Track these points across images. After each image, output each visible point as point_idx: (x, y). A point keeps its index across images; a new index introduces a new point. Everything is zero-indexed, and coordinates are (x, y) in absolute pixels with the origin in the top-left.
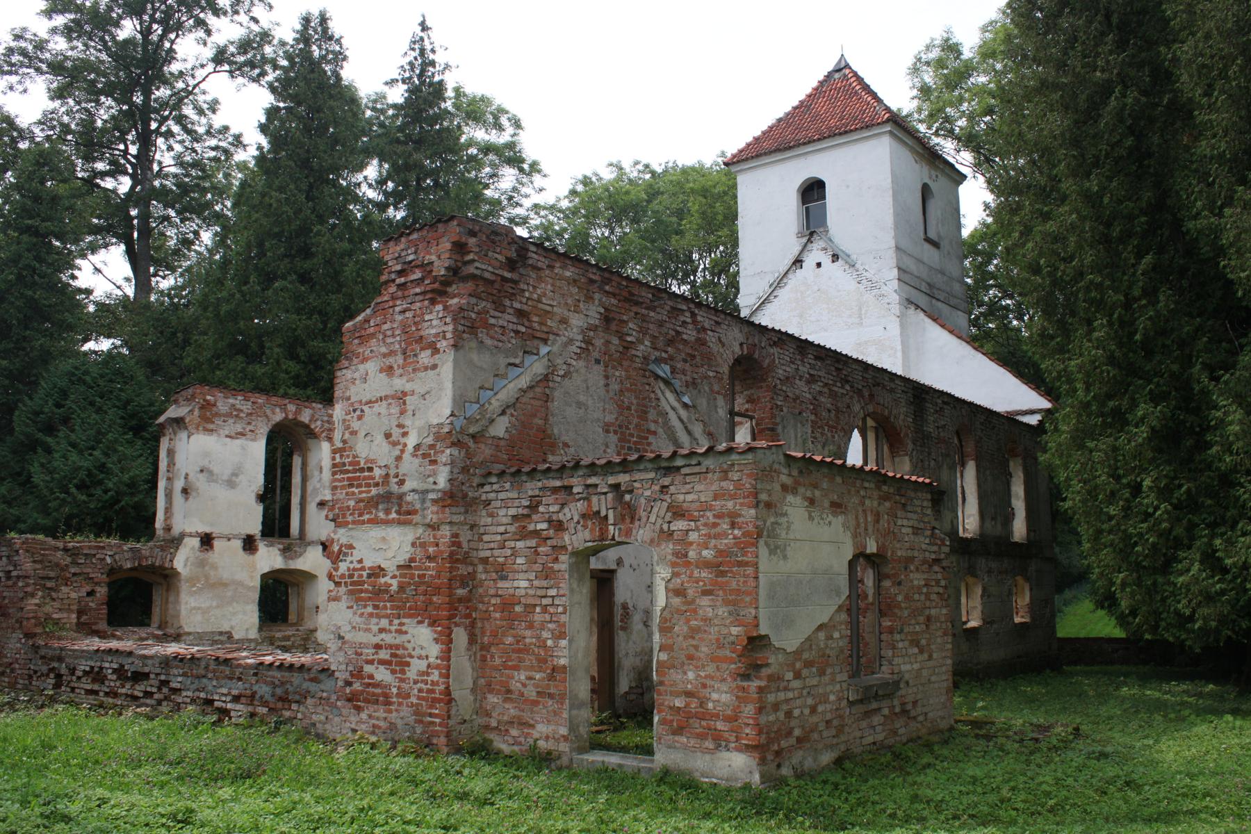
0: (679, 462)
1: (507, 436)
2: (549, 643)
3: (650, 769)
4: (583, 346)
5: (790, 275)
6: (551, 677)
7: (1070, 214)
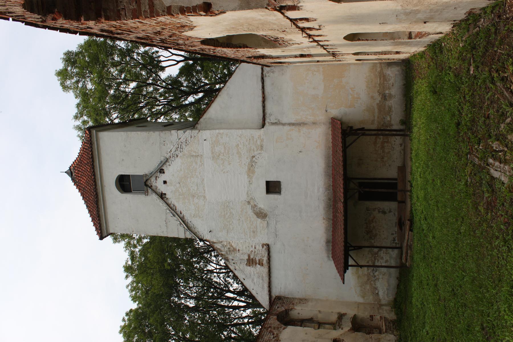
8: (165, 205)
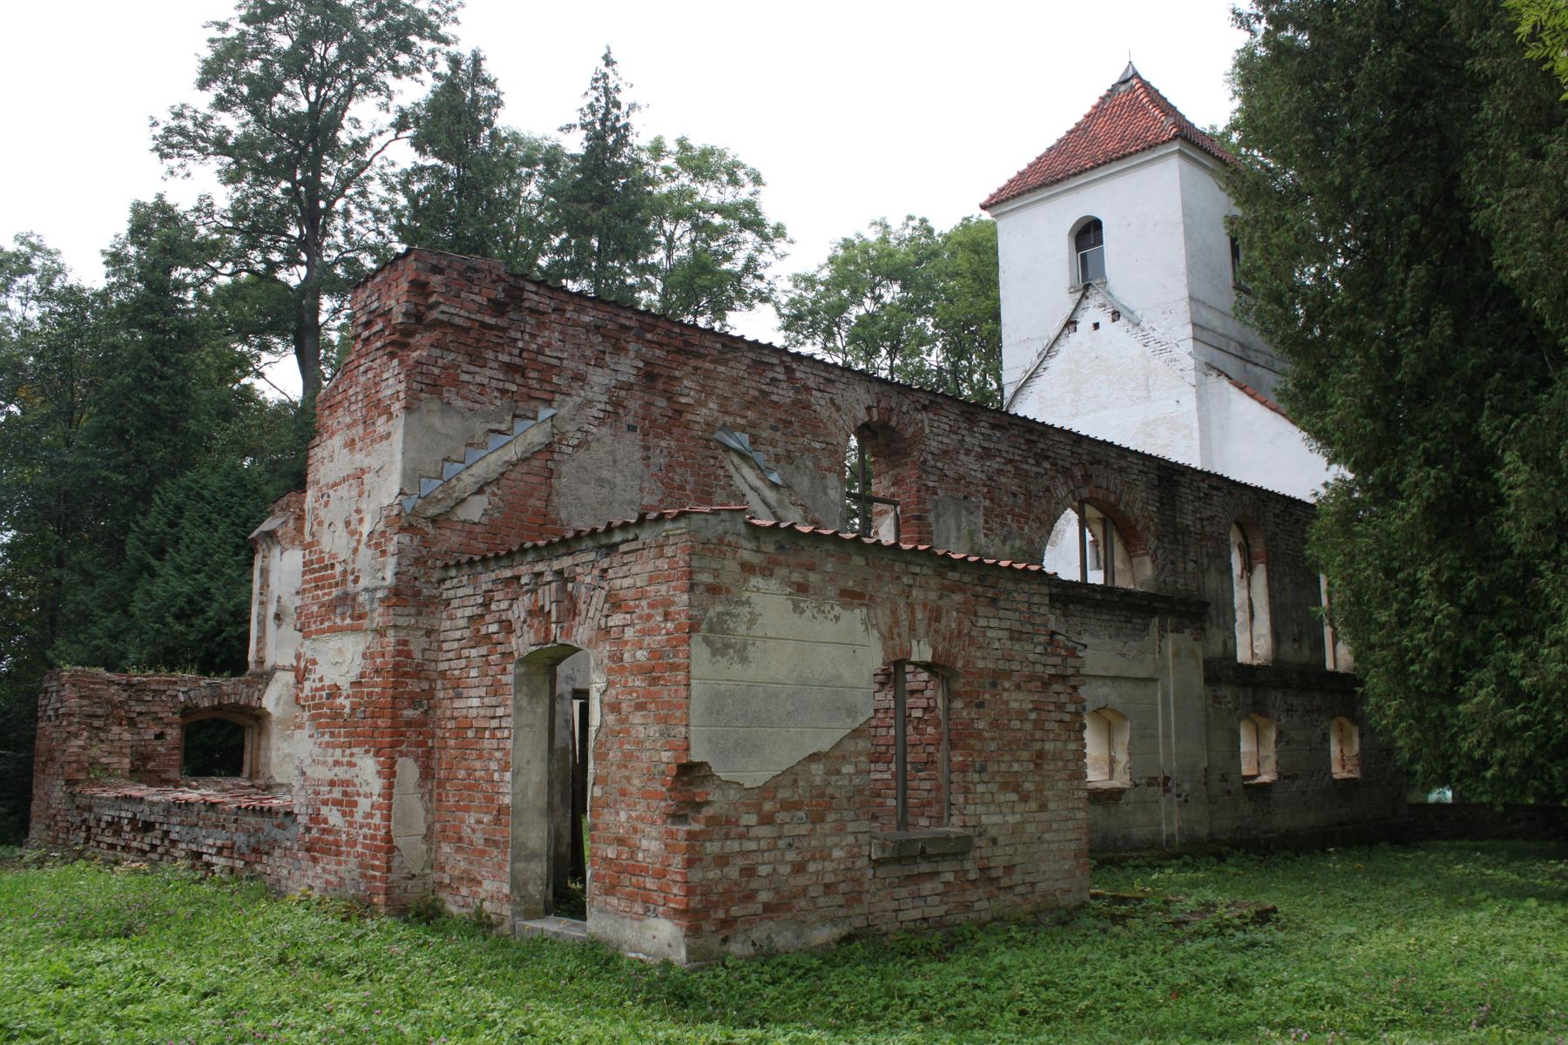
1: (485, 520)
2: (496, 776)
4: (609, 408)
5: (1062, 341)
6: (497, 821)
8: (1056, 333)
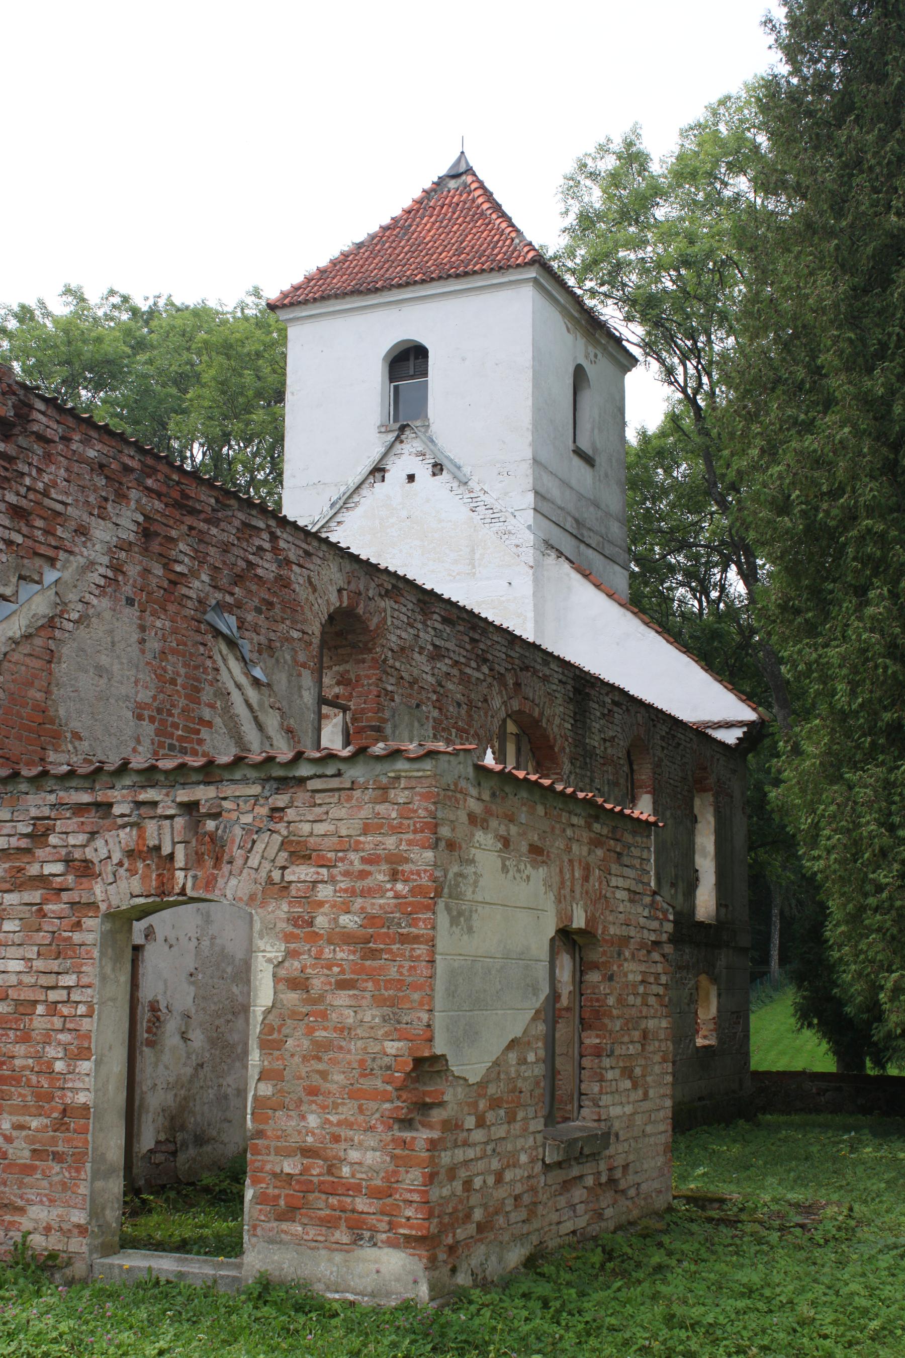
0: (304, 770)
2: (59, 1066)
3: (235, 1279)
4: (110, 574)
5: (364, 491)
6: (60, 1125)
7: (841, 427)
8: (358, 479)
